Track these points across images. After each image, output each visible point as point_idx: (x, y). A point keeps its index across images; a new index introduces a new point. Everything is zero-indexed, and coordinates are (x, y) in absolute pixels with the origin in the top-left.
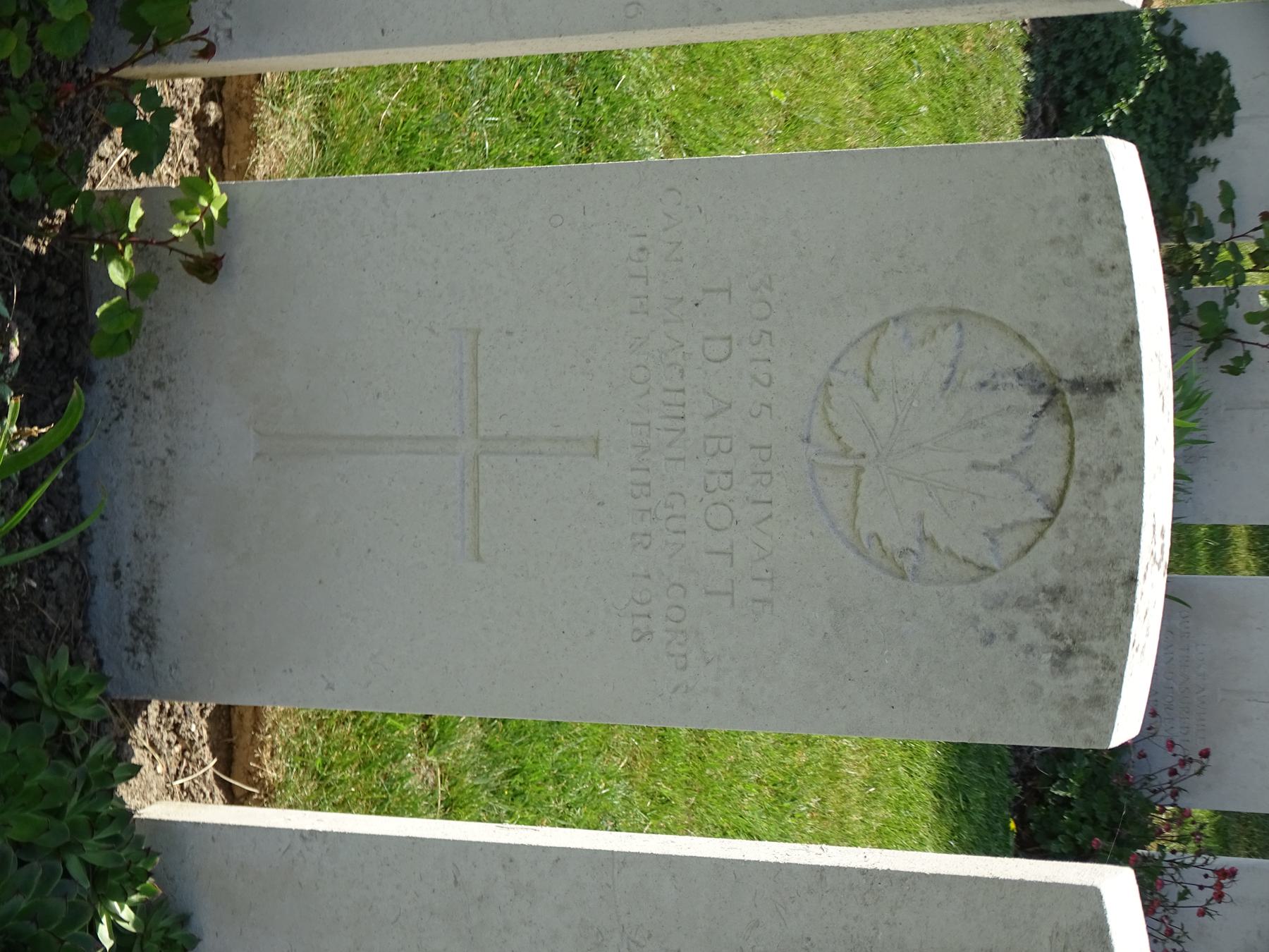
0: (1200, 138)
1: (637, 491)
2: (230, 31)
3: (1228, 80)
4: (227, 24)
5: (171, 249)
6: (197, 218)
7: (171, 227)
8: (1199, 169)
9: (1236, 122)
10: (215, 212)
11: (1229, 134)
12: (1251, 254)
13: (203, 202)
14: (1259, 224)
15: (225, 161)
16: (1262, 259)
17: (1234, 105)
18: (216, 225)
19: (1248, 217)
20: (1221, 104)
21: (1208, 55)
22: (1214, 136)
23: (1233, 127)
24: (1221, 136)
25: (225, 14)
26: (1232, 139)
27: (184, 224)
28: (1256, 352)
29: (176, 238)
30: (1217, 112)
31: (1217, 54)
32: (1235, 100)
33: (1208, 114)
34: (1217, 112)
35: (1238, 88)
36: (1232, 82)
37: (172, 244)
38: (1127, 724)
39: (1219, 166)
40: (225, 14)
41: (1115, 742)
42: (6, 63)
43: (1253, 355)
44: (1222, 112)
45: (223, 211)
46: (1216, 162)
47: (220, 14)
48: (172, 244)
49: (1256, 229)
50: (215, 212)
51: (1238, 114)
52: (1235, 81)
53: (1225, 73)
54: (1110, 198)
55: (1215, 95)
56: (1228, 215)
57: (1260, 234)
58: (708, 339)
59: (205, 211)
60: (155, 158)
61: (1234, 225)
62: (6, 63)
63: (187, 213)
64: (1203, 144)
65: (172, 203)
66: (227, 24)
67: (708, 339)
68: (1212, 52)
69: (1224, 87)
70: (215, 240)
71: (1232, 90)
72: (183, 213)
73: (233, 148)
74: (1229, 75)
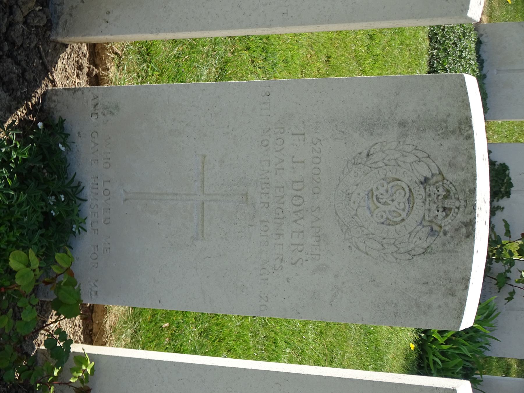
0: (497, 198)
1: (263, 186)
2: (97, 292)
3: (508, 175)
4: (96, 289)
5: (70, 386)
6: (81, 374)
7: (70, 379)
8: (496, 210)
9: (512, 192)
10: (89, 371)
11: (509, 197)
12: (517, 251)
13: (84, 368)
14: (521, 237)
15: (94, 319)
16: (521, 252)
17: (511, 185)
18: (89, 376)
19: (516, 234)
20: (506, 184)
21: (500, 164)
22: (502, 197)
23: (510, 194)
24: (505, 198)
25: (95, 285)
26: (510, 199)
27: (75, 377)
28: (517, 290)
29: (71, 382)
30: (504, 188)
31: (504, 164)
32: (511, 183)
33: (500, 189)
34: (504, 188)
35: (512, 178)
36: (510, 176)
37: (70, 384)
38: (468, 321)
39: (504, 210)
40: (95, 285)
41: (463, 327)
42: (3, 329)
43: (515, 290)
44: (506, 188)
45: (93, 369)
46: (503, 208)
47: (93, 285)
48: (70, 384)
49: (519, 240)
50: (89, 371)
51: (512, 189)
52: (511, 175)
53: (507, 172)
54: (467, 105)
55: (503, 180)
56: (508, 233)
57: (520, 242)
58: (294, 232)
59: (85, 371)
60: (64, 360)
61: (510, 237)
62: (3, 329)
63: (77, 373)
64: (498, 201)
65: (71, 369)
66: (96, 289)
67: (294, 232)
68: (502, 163)
69: (507, 178)
70: (89, 380)
71: (510, 179)
72: (75, 373)
73: (97, 314)
74: (509, 173)
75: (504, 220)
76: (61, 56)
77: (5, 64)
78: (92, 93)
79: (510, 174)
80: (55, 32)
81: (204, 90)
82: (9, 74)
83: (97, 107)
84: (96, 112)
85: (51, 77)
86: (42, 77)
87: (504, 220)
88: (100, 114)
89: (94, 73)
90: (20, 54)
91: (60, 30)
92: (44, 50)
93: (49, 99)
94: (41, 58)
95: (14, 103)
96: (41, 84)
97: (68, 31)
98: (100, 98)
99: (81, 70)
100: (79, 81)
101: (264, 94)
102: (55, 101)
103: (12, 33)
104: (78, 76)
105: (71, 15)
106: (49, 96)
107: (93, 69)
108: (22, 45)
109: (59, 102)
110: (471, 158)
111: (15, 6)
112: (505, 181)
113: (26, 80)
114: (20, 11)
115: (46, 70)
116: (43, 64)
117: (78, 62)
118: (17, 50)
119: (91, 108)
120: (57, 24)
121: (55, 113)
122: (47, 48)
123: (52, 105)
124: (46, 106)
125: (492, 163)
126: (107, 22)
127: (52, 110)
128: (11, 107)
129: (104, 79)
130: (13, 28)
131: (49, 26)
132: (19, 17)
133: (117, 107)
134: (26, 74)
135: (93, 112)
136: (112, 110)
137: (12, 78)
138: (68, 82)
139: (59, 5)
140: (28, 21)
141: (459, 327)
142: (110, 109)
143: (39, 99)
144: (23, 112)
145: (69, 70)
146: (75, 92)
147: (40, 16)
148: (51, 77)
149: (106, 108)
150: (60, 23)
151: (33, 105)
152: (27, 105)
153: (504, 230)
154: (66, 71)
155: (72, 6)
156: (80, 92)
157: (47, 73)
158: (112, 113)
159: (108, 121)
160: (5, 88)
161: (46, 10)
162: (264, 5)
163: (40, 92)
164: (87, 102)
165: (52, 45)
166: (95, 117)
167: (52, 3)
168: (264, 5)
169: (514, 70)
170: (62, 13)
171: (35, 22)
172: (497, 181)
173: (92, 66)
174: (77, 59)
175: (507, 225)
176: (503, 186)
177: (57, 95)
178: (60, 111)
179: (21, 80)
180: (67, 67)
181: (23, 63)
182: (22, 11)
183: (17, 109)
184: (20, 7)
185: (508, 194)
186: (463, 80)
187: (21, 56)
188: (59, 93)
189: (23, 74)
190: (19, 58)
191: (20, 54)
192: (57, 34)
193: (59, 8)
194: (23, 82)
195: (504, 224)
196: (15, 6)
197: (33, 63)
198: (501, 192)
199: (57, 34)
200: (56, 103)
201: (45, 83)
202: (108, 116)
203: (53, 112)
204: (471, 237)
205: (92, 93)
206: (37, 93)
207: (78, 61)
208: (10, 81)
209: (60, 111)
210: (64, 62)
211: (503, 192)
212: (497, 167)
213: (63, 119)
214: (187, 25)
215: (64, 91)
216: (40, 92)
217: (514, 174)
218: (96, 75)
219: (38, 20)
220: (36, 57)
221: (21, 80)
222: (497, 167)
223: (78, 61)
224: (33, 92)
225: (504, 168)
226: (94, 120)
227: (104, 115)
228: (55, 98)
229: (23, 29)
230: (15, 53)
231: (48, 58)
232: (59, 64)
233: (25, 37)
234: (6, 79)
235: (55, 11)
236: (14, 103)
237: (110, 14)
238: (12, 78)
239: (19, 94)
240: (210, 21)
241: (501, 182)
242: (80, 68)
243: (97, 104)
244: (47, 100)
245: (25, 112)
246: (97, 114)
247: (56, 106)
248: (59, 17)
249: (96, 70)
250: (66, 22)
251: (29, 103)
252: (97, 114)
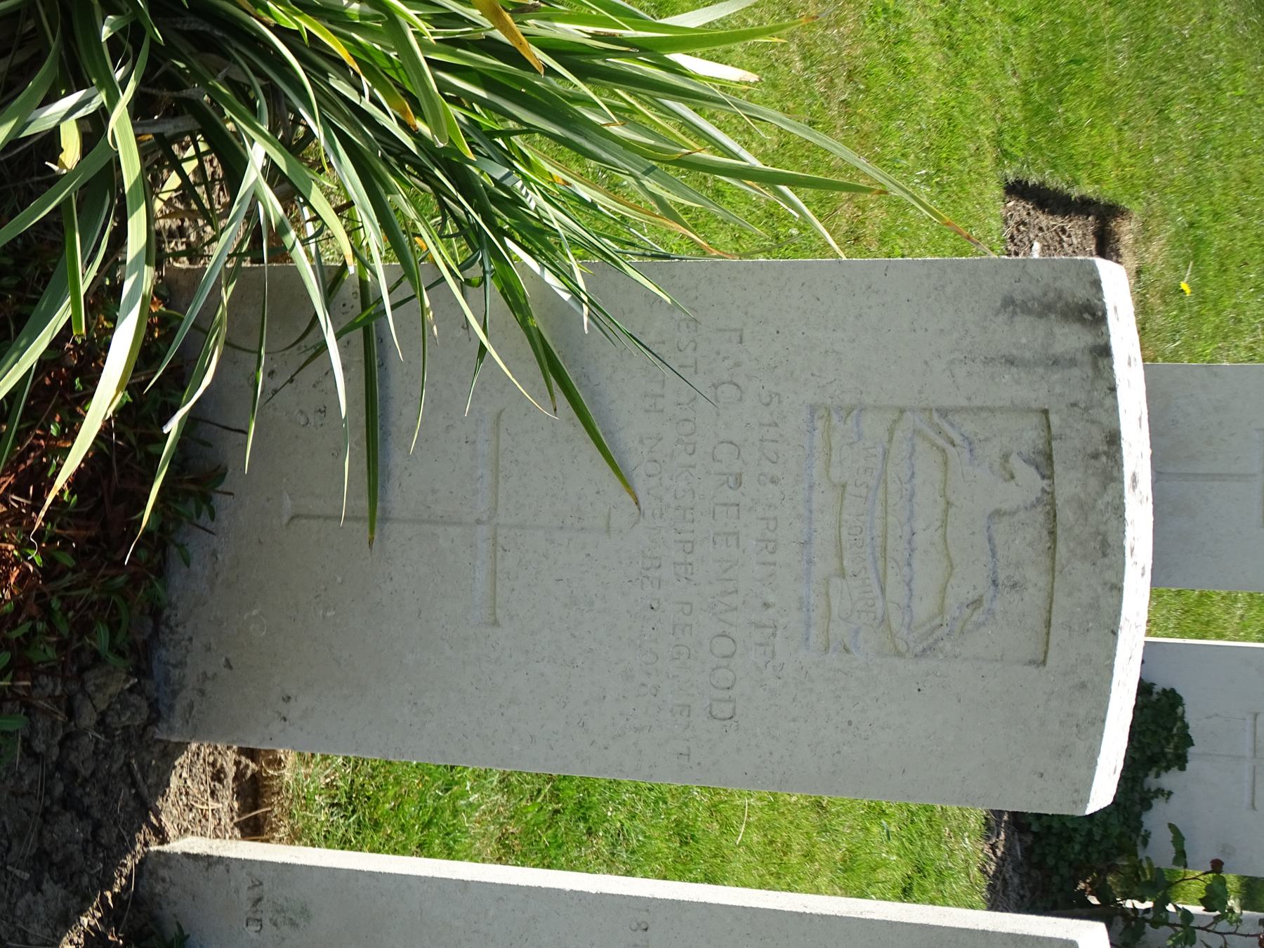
0: (1155, 769)
11: (1182, 768)
17: (1188, 741)
20: (1176, 739)
21: (1164, 690)
22: (1167, 769)
24: (1175, 769)
30: (1172, 745)
31: (1173, 691)
33: (1163, 748)
35: (1191, 725)
38: (1102, 792)
39: (1172, 797)
41: (1091, 809)
44: (1176, 748)
46: (1170, 793)
51: (1191, 750)
52: (1189, 718)
53: (1180, 710)
55: (1171, 729)
56: (1181, 857)
64: (1158, 775)
68: (1168, 689)
69: (1179, 724)
71: (1186, 726)
75: (1171, 826)
76: (176, 763)
77: (56, 828)
78: (249, 874)
79: (1186, 715)
80: (165, 726)
81: (501, 898)
82: (64, 845)
83: (261, 906)
84: (258, 917)
85: (154, 821)
86: (136, 826)
87: (1171, 826)
88: (266, 922)
89: (249, 773)
90: (89, 794)
91: (177, 723)
92: (141, 767)
93: (151, 874)
94: (134, 784)
95: (74, 902)
96: (133, 843)
97: (195, 728)
98: (266, 887)
99: (220, 781)
100: (216, 806)
101: (634, 926)
102: (163, 880)
103: (72, 757)
104: (213, 793)
105: (202, 692)
106: (150, 866)
107: (247, 766)
108: (93, 774)
109: (172, 883)
110: (1105, 544)
111: (80, 696)
112: (1175, 731)
113: (101, 845)
114: (90, 706)
115: (143, 809)
116: (138, 796)
117: (213, 764)
118: (82, 786)
119: (247, 907)
120: (171, 708)
121: (164, 905)
122: (148, 758)
123: (159, 888)
124: (143, 887)
125: (1144, 689)
126: (285, 719)
127: (157, 899)
128: (68, 910)
129: (271, 786)
130: (75, 743)
131: (156, 715)
132: (88, 718)
133: (304, 911)
134: (103, 832)
135: (251, 915)
136: (293, 917)
137: (72, 854)
138: (191, 815)
139: (175, 666)
140: (108, 720)
141: (1086, 801)
142: (290, 915)
143: (129, 878)
144: (94, 917)
145: (194, 790)
146: (210, 865)
147: (134, 705)
148: (154, 821)
149: (280, 910)
150: (178, 707)
151: (114, 896)
152: (104, 898)
153: (1171, 852)
154: (187, 794)
155: (205, 673)
156: (222, 868)
157: (148, 816)
158: (293, 924)
159: (283, 939)
160: (55, 873)
161: (149, 686)
162: (636, 730)
163: (130, 862)
164: (237, 891)
165: (156, 750)
166: (254, 928)
167: (160, 661)
168: (636, 730)
169: (1196, 475)
170: (183, 687)
171: (124, 719)
172: (1155, 733)
173: (243, 759)
174: (211, 759)
175: (1178, 838)
176: (1168, 743)
177: (170, 868)
178: (176, 904)
179: (90, 849)
180: (189, 783)
181: (96, 813)
182: (94, 706)
183: (82, 912)
184: (89, 696)
185: (1180, 761)
186: (1093, 270)
187: (92, 797)
188: (173, 863)
189: (95, 833)
190: (86, 801)
191: (89, 794)
192: (171, 729)
193: (175, 673)
194: (94, 850)
195: (1170, 835)
196: (80, 696)
197: (116, 802)
198: (1164, 754)
199: (171, 729)
200: (167, 885)
201: (142, 838)
202: (286, 929)
203: (159, 904)
204: (1133, 273)
205: (249, 874)
206: (125, 866)
207: (215, 761)
208: (69, 859)
209: (176, 904)
210: (184, 775)
211: (1170, 756)
212: (1155, 697)
213: (186, 933)
214: (465, 750)
215: (185, 860)
216: (130, 862)
217: (1194, 716)
218: (253, 775)
219: (128, 714)
220: (122, 785)
221: (90, 849)
222: (1155, 697)
223: (215, 761)
224: (115, 866)
225: (1172, 700)
226: (254, 935)
227: (275, 925)
228: (163, 873)
229: (98, 739)
230: (78, 793)
231: (150, 781)
232: (174, 782)
233: (101, 757)
234: (57, 858)
235: (167, 679)
236: (74, 902)
237: (292, 702)
238: (72, 854)
239: (85, 880)
240: (516, 748)
241: (1165, 734)
242: (218, 776)
243: (260, 899)
244: (146, 875)
245: (99, 915)
246: (260, 920)
247: (166, 891)
248: (175, 694)
249: (252, 765)
250: (191, 706)
251: (109, 894)
252: (260, 920)
